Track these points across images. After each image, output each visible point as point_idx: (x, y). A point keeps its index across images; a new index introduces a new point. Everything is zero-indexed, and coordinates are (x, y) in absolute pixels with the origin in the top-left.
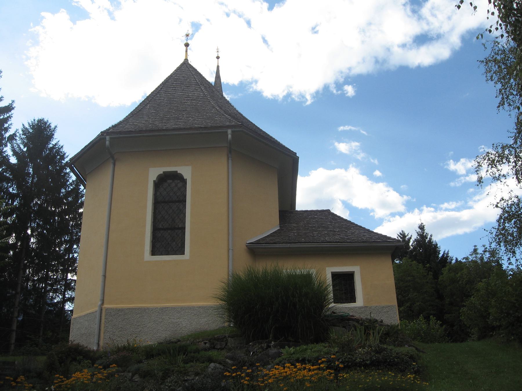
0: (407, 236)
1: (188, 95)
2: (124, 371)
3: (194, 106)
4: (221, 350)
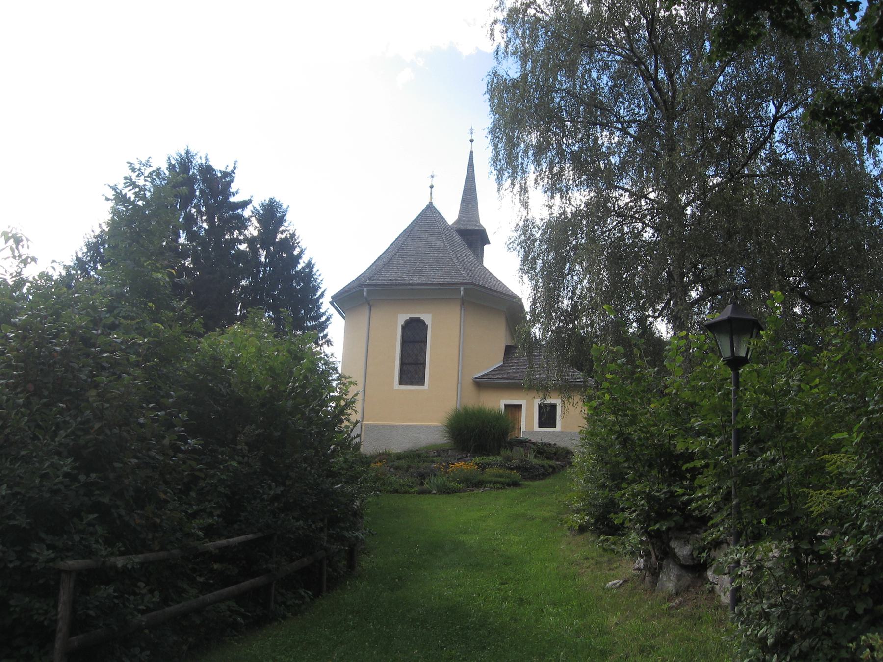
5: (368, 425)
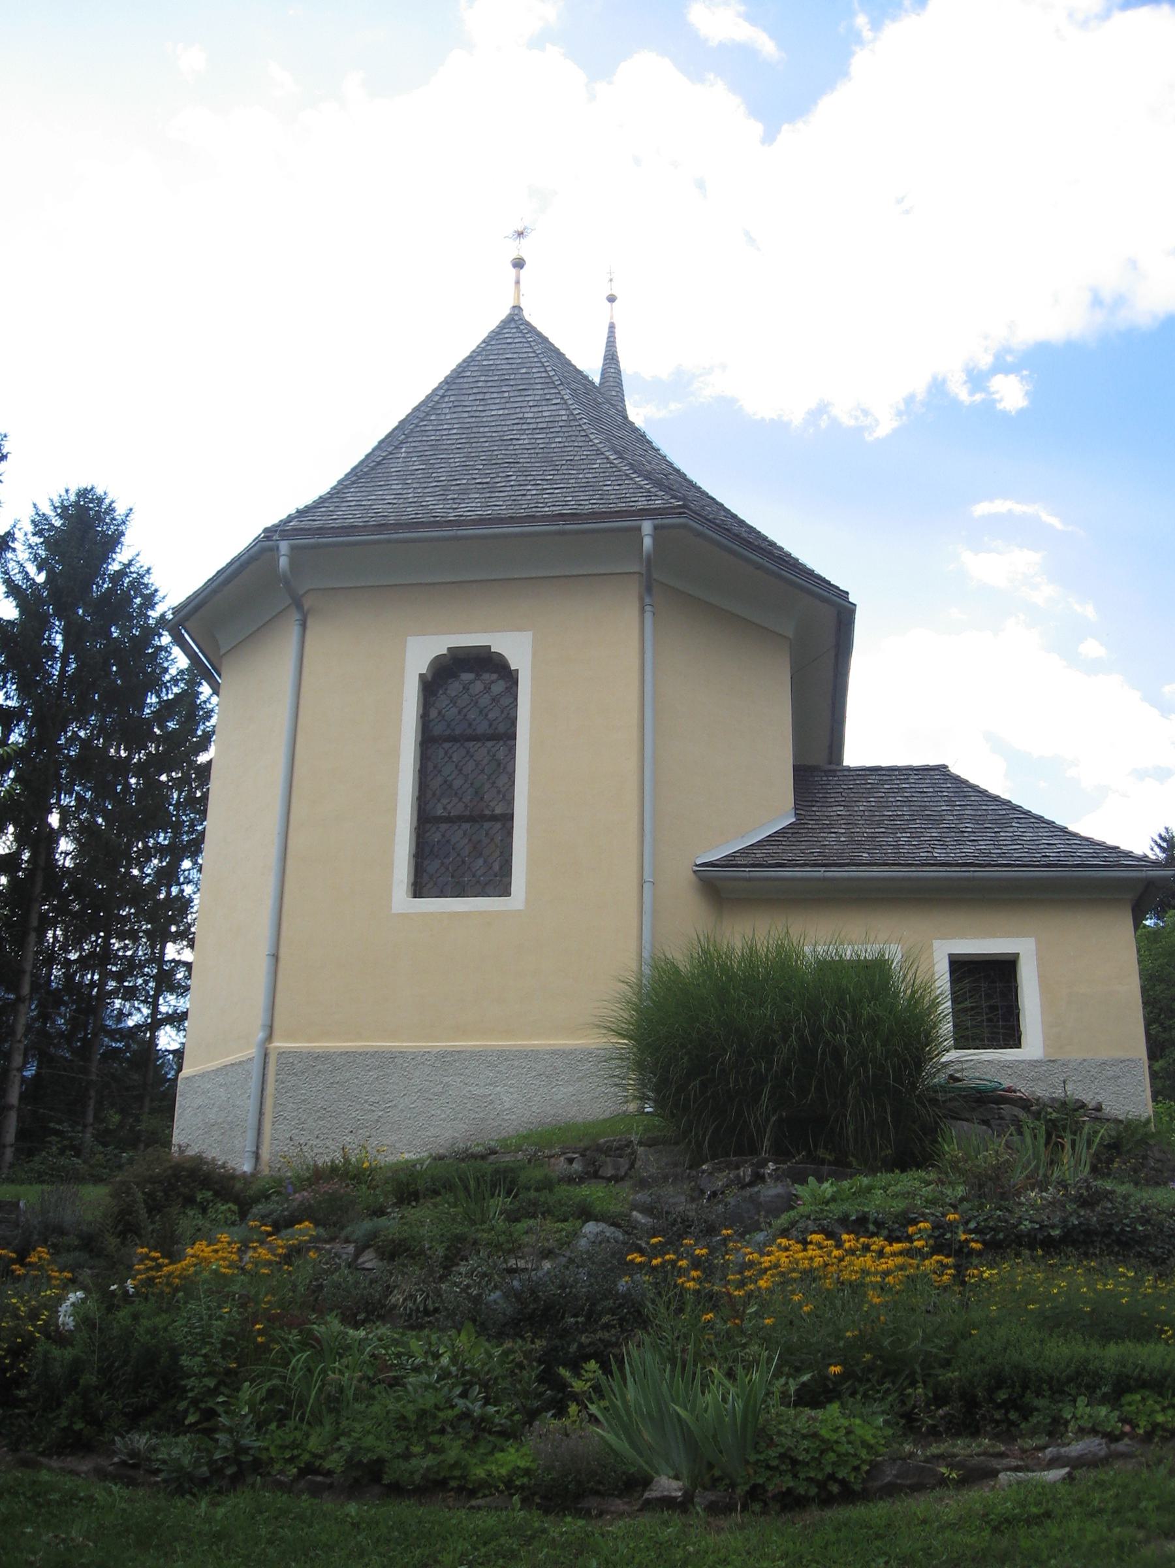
1: (521, 415)
2: (332, 1240)
3: (541, 451)
4: (617, 1182)
5: (298, 1054)
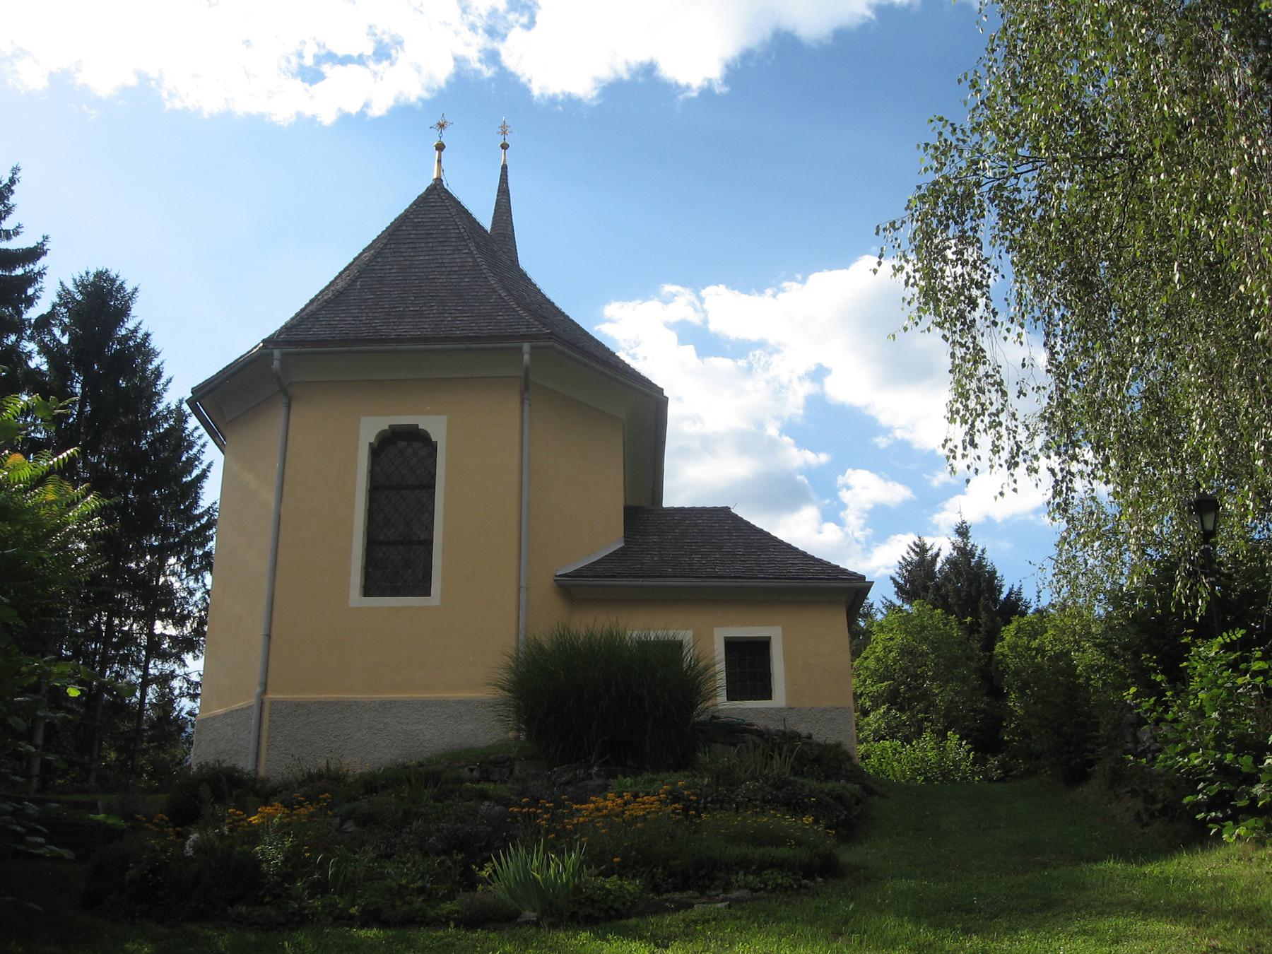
0: (929, 549)
1: (440, 261)
